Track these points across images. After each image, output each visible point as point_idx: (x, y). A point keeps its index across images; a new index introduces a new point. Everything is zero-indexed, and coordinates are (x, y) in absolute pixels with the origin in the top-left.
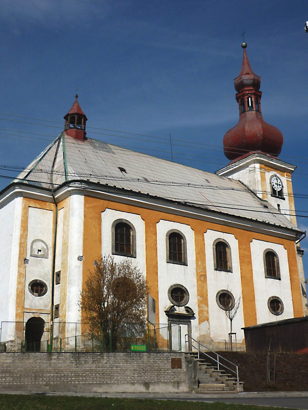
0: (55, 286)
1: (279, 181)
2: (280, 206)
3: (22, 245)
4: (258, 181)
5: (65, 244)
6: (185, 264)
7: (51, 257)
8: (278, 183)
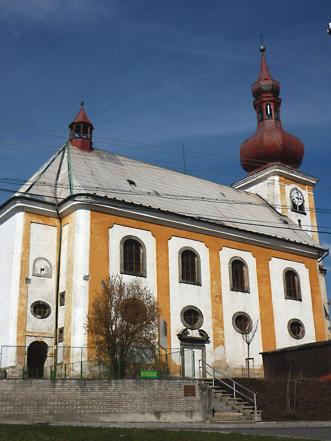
0: (59, 307)
1: (300, 194)
2: (301, 221)
3: (24, 264)
4: (277, 194)
5: (70, 263)
6: (199, 284)
7: (54, 276)
8: (299, 197)
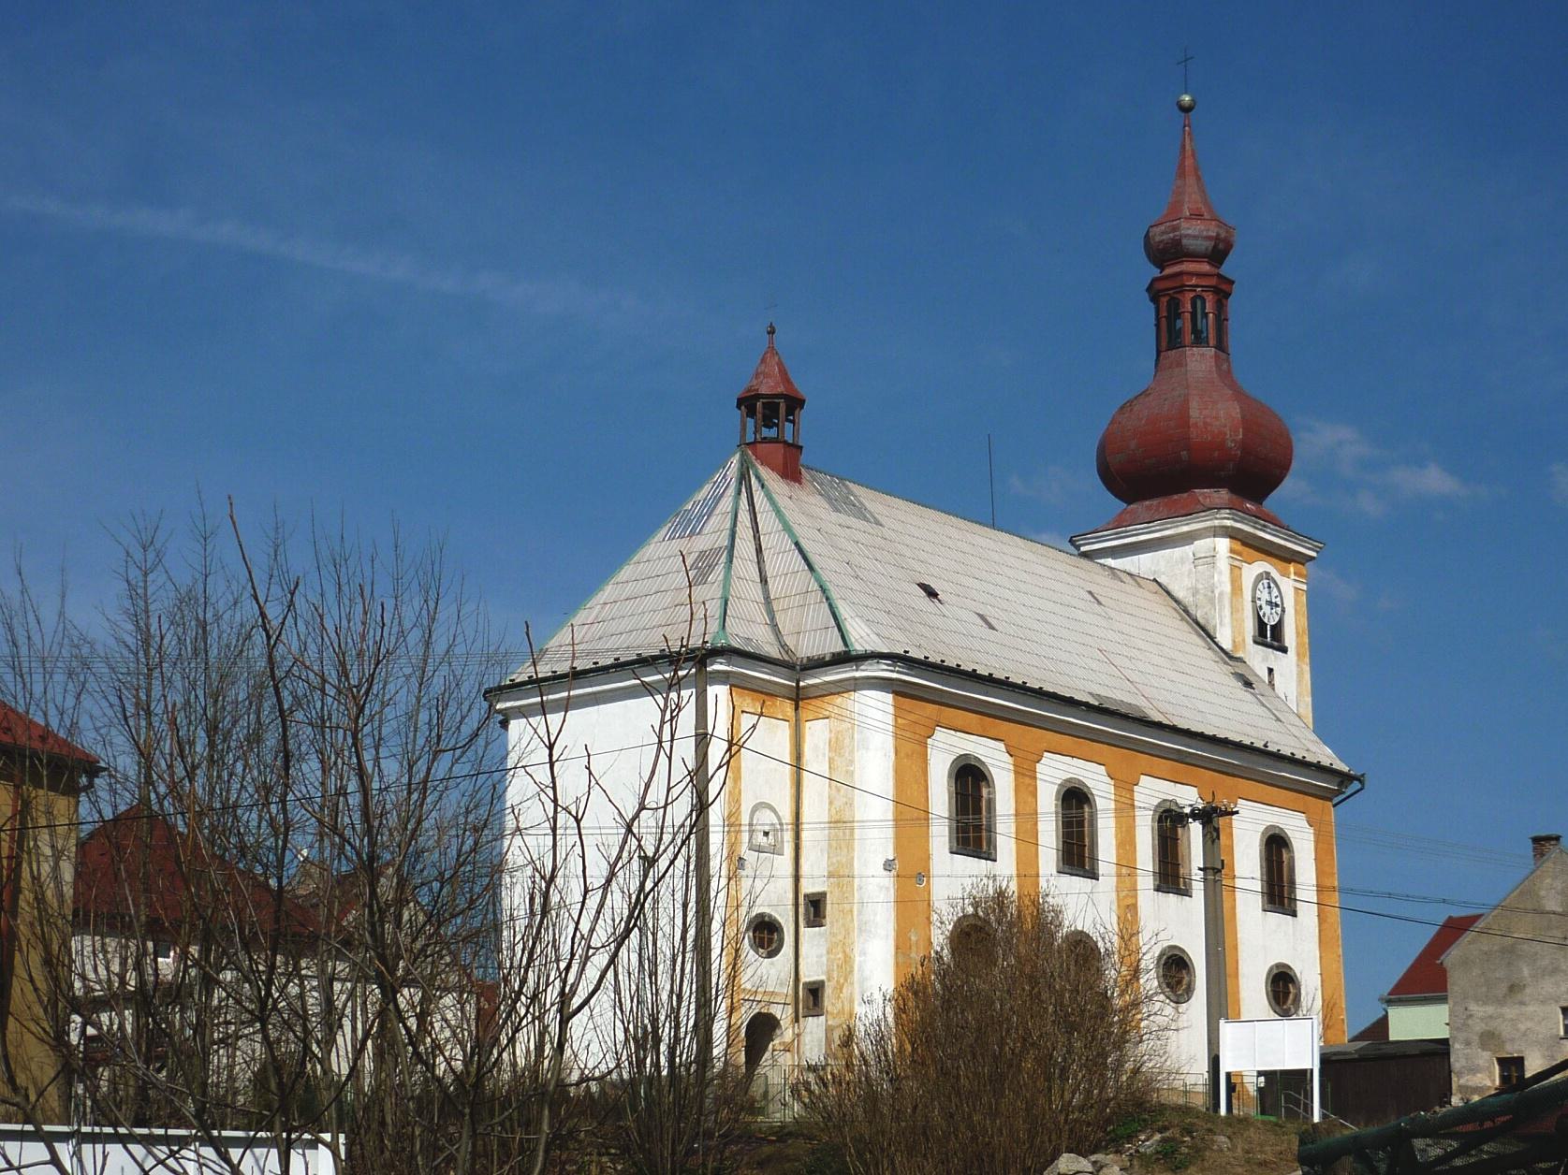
0: (802, 929)
1: (1275, 592)
2: (1275, 672)
4: (1221, 594)
6: (1093, 875)
8: (1273, 601)
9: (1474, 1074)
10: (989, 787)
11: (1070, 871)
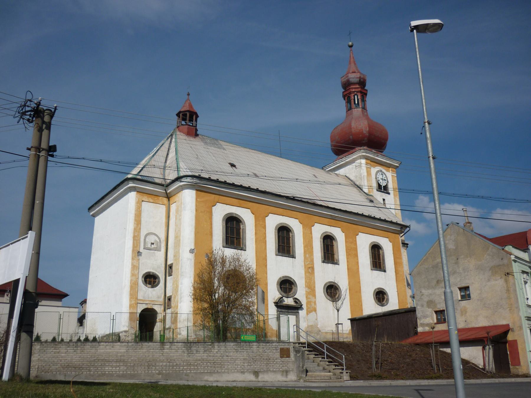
1: (384, 176)
3: (136, 239)
4: (364, 176)
6: (293, 257)
8: (384, 178)
9: (426, 318)
10: (243, 224)
11: (282, 255)
